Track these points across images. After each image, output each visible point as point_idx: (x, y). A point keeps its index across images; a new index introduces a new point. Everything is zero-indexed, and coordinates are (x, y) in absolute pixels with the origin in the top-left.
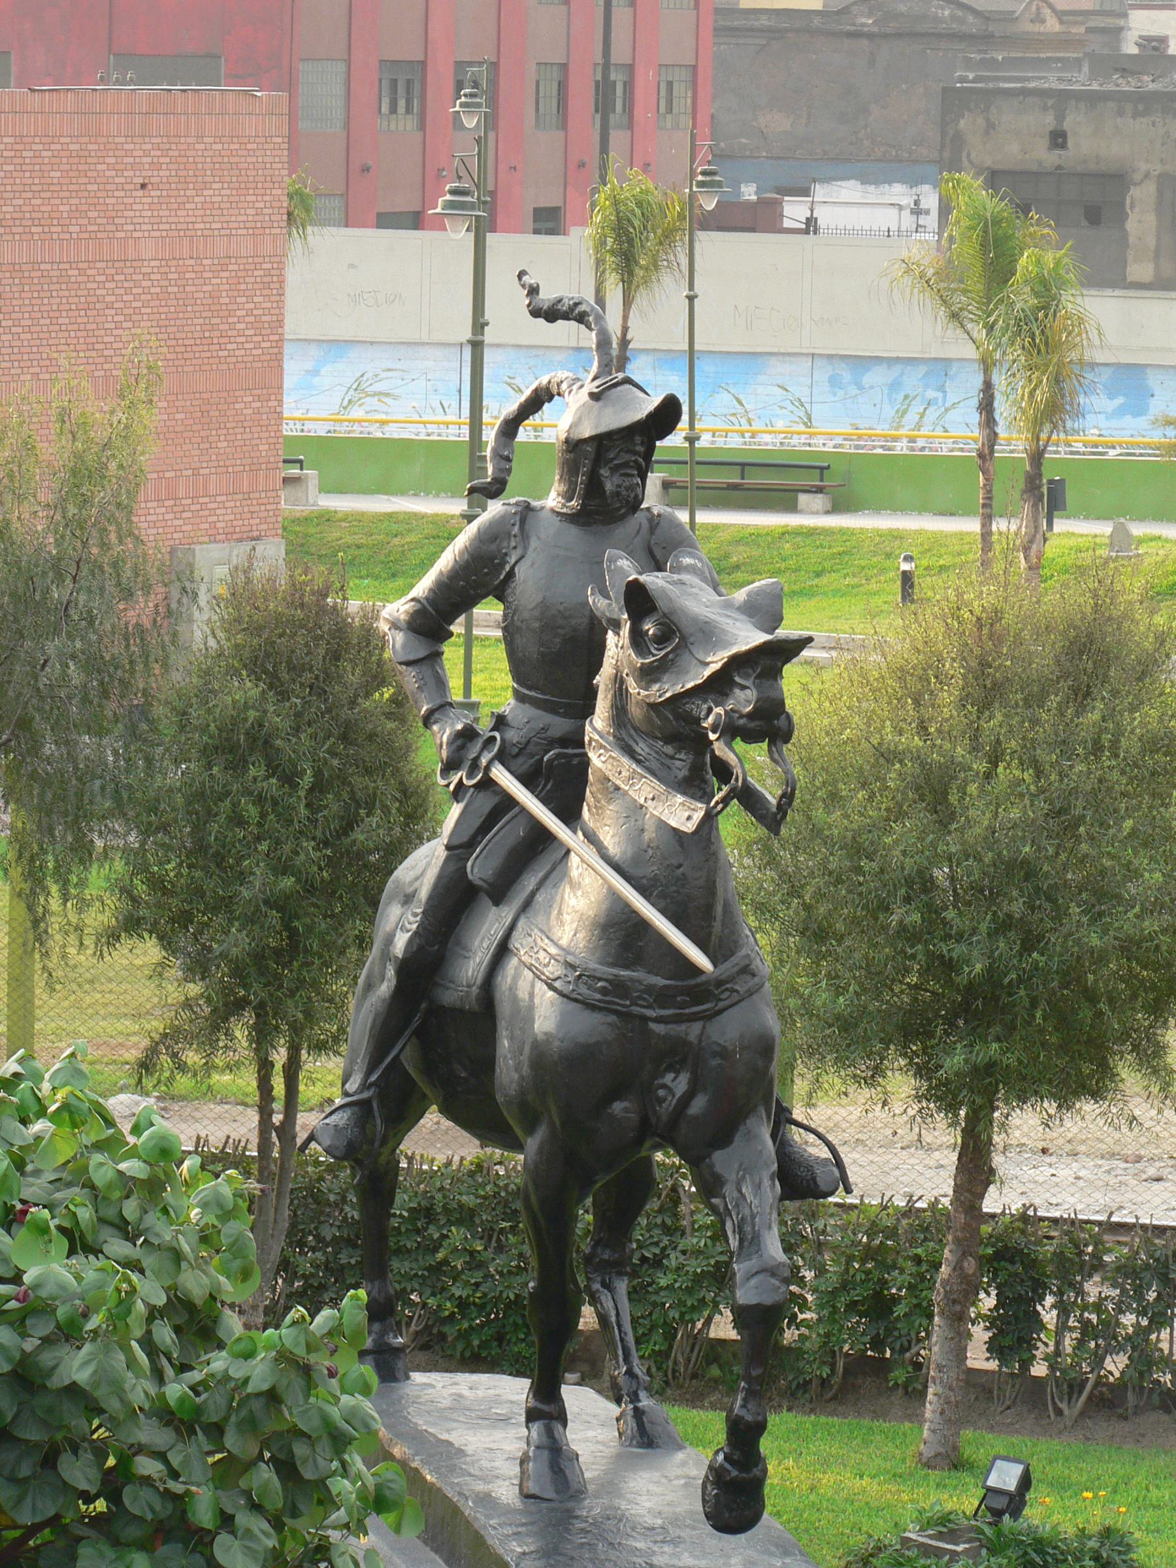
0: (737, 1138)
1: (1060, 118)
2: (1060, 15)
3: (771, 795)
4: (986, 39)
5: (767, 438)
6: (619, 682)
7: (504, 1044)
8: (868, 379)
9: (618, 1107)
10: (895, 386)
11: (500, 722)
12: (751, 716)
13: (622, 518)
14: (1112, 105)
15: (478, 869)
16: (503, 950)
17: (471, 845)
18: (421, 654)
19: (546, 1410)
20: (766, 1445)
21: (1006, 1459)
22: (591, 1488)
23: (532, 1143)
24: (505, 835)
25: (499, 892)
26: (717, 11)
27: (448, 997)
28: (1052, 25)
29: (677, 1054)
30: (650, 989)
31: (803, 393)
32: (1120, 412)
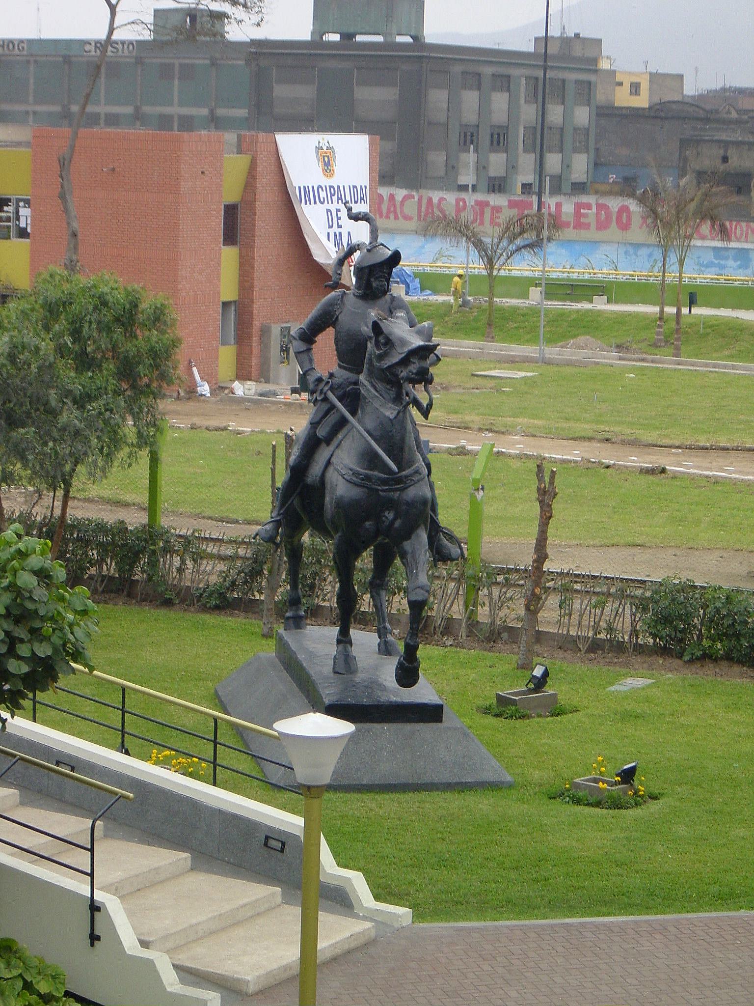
0: (413, 537)
1: (726, 151)
2: (738, 112)
3: (425, 403)
4: (707, 120)
5: (600, 275)
6: (370, 359)
7: (327, 499)
8: (640, 253)
9: (367, 524)
10: (650, 255)
11: (331, 375)
12: (416, 374)
13: (379, 297)
14: (746, 147)
15: (321, 432)
16: (329, 463)
17: (319, 423)
18: (304, 349)
19: (344, 639)
20: (419, 653)
21: (540, 664)
22: (360, 670)
23: (336, 537)
24: (332, 419)
25: (328, 440)
26: (598, 107)
27: (309, 480)
28: (734, 115)
29: (391, 504)
30: (379, 479)
31: (614, 257)
32: (739, 267)
